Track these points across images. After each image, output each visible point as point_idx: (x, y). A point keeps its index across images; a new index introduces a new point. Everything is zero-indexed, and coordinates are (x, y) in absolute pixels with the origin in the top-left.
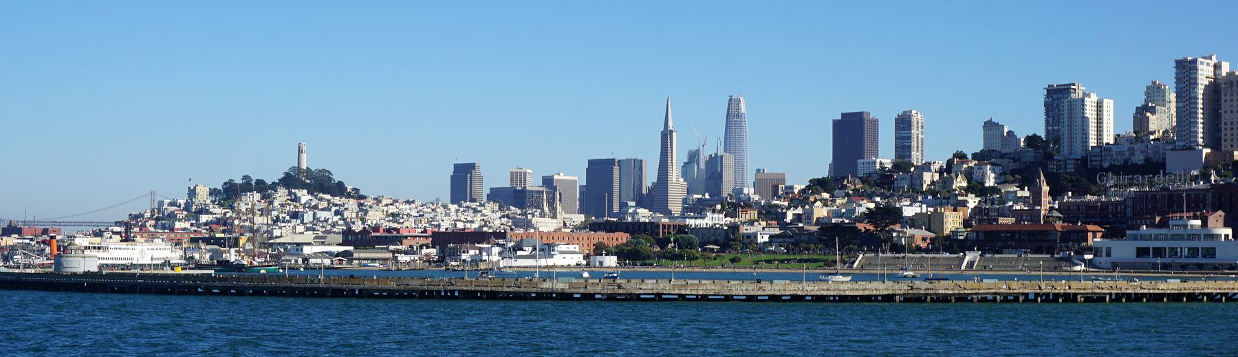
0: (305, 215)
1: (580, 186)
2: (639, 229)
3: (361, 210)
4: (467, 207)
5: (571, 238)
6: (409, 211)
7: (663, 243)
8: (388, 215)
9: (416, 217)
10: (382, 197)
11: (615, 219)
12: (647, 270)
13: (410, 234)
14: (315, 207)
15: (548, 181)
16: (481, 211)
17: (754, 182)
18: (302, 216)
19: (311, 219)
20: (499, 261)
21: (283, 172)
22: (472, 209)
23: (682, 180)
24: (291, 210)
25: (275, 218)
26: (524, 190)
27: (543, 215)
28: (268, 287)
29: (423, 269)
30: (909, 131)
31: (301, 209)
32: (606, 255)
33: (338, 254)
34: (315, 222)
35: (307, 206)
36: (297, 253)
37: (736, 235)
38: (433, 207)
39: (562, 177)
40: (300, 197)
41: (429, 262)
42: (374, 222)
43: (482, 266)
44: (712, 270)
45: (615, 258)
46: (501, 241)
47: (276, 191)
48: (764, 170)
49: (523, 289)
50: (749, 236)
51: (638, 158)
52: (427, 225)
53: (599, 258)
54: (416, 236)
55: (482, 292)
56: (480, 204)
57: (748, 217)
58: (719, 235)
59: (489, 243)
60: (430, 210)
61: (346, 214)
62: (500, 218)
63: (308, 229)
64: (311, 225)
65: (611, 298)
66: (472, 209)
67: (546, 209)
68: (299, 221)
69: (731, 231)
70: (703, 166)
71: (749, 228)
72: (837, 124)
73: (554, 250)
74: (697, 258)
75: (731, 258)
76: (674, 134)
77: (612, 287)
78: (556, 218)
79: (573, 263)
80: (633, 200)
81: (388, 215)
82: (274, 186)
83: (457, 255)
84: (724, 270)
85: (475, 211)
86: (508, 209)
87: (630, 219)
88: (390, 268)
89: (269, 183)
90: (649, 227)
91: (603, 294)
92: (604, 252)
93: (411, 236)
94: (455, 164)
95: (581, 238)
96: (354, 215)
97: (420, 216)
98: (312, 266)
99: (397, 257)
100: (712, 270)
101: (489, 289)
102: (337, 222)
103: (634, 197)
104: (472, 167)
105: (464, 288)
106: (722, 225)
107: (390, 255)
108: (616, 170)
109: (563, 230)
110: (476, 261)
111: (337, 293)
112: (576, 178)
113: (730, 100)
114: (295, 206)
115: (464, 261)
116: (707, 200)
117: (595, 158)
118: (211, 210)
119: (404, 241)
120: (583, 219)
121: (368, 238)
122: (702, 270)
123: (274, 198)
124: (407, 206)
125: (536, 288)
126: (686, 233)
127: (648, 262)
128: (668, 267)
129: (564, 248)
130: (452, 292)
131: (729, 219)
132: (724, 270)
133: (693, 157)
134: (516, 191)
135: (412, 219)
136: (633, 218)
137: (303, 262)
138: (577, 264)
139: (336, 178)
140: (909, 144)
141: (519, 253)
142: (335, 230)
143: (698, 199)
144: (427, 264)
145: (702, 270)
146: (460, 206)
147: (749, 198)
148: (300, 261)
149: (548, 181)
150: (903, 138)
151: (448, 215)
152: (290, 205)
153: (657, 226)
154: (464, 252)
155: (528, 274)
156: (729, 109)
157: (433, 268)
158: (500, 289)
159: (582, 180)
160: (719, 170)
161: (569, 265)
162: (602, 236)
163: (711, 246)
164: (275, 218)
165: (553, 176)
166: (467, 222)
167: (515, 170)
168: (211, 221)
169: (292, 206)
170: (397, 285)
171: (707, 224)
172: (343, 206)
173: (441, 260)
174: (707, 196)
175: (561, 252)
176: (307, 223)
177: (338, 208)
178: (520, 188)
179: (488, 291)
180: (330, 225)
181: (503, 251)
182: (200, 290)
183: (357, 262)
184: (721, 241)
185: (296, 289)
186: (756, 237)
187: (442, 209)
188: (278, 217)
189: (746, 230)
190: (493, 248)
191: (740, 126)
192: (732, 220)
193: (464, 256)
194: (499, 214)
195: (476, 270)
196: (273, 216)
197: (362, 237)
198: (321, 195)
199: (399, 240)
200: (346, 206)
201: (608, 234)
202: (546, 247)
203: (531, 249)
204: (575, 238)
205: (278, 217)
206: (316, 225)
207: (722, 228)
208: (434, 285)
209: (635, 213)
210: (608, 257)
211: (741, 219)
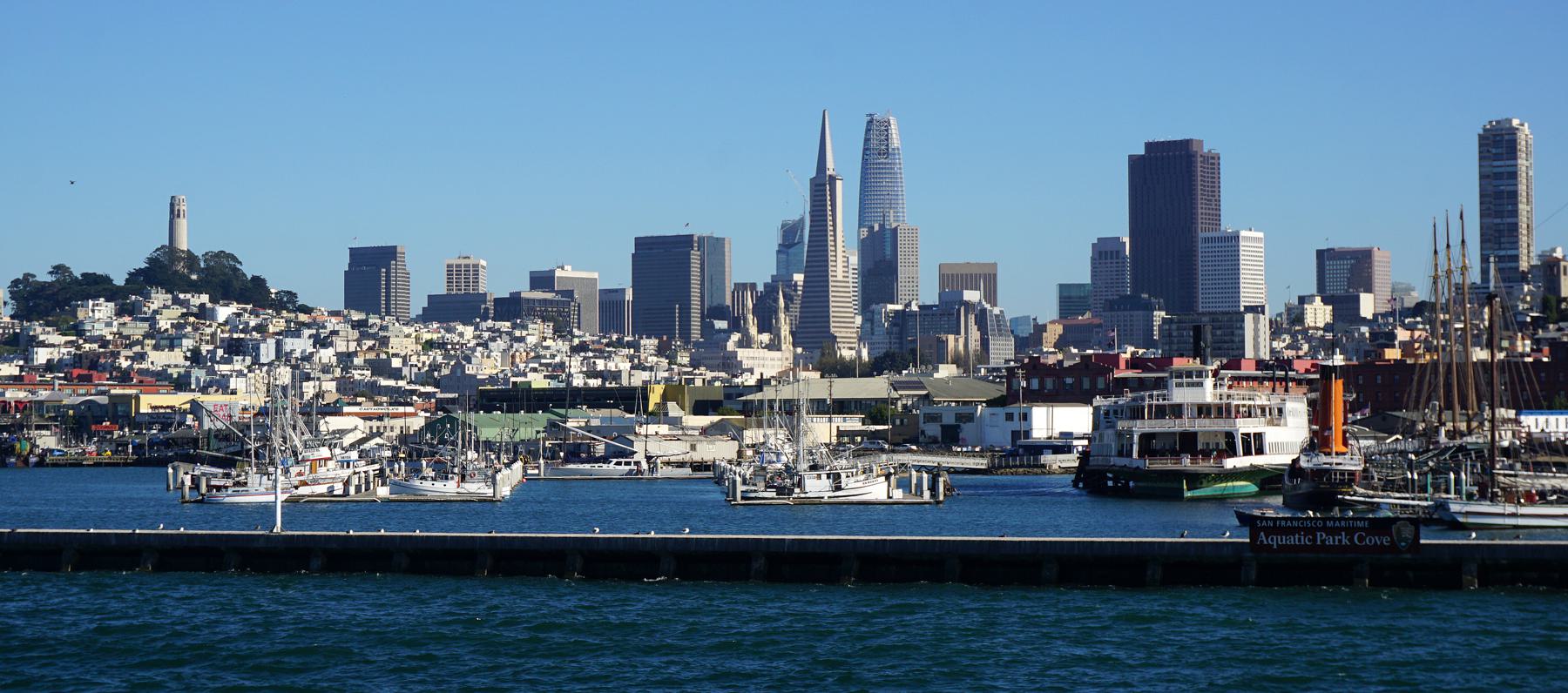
30: (1512, 162)
72: (1135, 163)
76: (839, 183)
78: (779, 349)
104: (386, 255)
108: (695, 255)
112: (596, 275)
113: (870, 122)
117: (650, 234)
118: (42, 338)
139: (249, 270)
140: (1512, 188)
150: (1498, 176)
156: (867, 140)
160: (888, 251)
165: (553, 271)
167: (455, 262)
168: (60, 360)
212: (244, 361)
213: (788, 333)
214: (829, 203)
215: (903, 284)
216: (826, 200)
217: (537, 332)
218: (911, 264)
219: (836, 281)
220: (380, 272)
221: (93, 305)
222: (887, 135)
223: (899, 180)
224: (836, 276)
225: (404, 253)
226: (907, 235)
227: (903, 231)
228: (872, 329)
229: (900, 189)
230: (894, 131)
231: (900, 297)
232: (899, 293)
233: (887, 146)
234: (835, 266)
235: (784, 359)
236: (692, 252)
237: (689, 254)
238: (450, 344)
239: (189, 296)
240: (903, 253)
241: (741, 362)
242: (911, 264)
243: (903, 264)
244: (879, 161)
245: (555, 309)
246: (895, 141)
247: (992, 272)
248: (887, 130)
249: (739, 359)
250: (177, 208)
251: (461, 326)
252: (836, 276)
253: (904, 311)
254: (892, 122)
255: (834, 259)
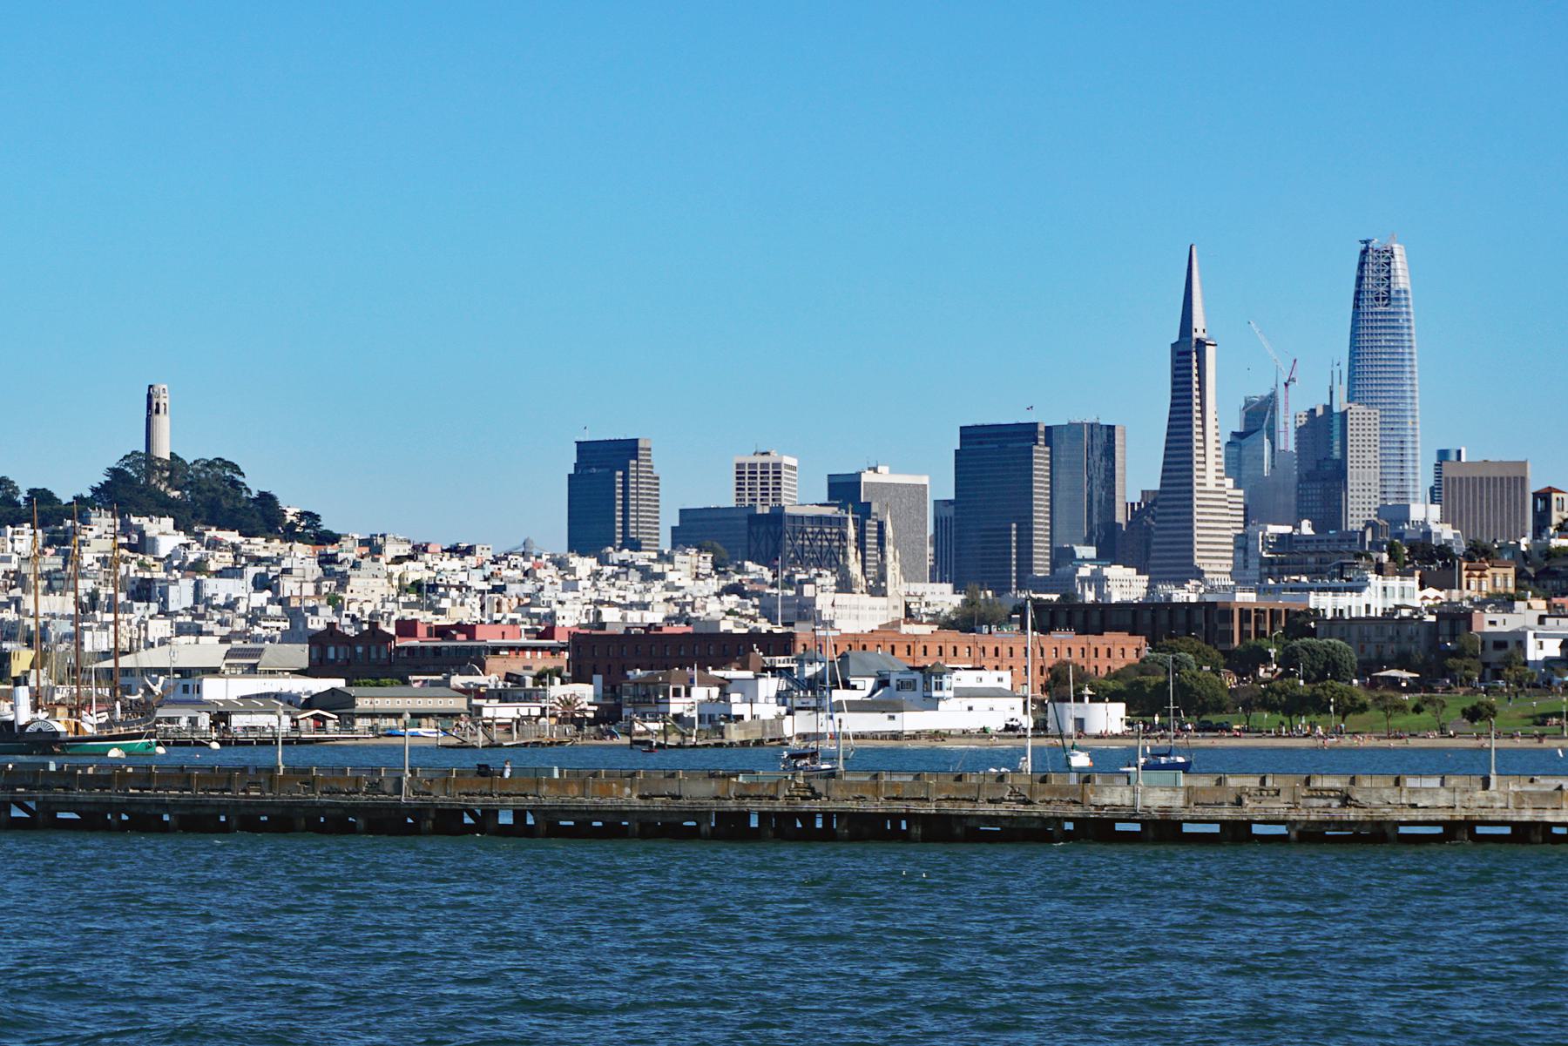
0: (172, 590)
1: (938, 504)
2: (1171, 625)
3: (328, 574)
4: (622, 564)
5: (977, 653)
6: (463, 577)
7: (1246, 662)
8: (403, 590)
9: (482, 592)
10: (383, 536)
11: (1055, 597)
12: (1218, 743)
13: (508, 641)
14: (199, 567)
15: (844, 489)
16: (661, 576)
17: (1432, 490)
18: (164, 593)
19: (189, 602)
20: (779, 718)
21: (103, 469)
22: (638, 568)
23: (1229, 482)
24: (132, 575)
25: (85, 599)
26: (777, 516)
27: (845, 585)
28: (237, 805)
29: (560, 743)
31: (159, 574)
32: (1093, 699)
33: (311, 702)
34: (201, 609)
35: (176, 563)
36: (185, 697)
37: (1463, 638)
38: (527, 565)
39: (885, 476)
40: (154, 539)
41: (579, 723)
42: (368, 609)
43: (734, 734)
44: (1413, 742)
45: (1119, 709)
46: (781, 662)
47: (85, 521)
48: (1459, 452)
49: (1039, 809)
50: (1500, 643)
51: (1104, 422)
52: (518, 616)
53: (1072, 710)
54: (524, 648)
55: (910, 817)
56: (661, 554)
57: (1486, 586)
58: (1411, 638)
59: (744, 667)
60: (518, 574)
61: (288, 586)
62: (718, 595)
63: (181, 630)
64: (189, 619)
65: (1312, 835)
66: (638, 568)
67: (855, 568)
68: (154, 607)
69: (1445, 627)
70: (1288, 441)
71: (1499, 617)
73: (939, 687)
74: (1363, 708)
75: (1467, 706)
76: (1210, 351)
77: (1323, 802)
78: (884, 595)
79: (996, 723)
80: (1088, 542)
81: (403, 590)
82: (81, 508)
83: (657, 702)
84: (1447, 743)
85: (647, 575)
86: (740, 570)
87: (1090, 597)
88: (469, 739)
89: (66, 498)
90: (1200, 617)
91: (1291, 824)
92: (1087, 691)
93: (511, 648)
94: (578, 443)
95: (1005, 651)
96: (309, 589)
97: (495, 589)
98: (241, 736)
99: (479, 709)
100: (1413, 742)
101: (931, 808)
102: (263, 610)
103: (1091, 533)
104: (627, 450)
105: (853, 806)
106: (1416, 610)
107: (460, 704)
108: (1041, 454)
109: (905, 629)
110: (716, 719)
111: (447, 822)
113: (1364, 252)
114: (142, 565)
115: (678, 718)
116: (1308, 540)
119: (491, 662)
120: (957, 600)
121: (383, 656)
122: (1384, 743)
123: (83, 543)
124: (456, 563)
125: (1081, 804)
126: (1312, 633)
127: (1215, 719)
128: (1278, 736)
129: (968, 679)
130: (809, 817)
131: (1431, 592)
132: (1447, 743)
133: (1259, 416)
134: (754, 519)
135: (473, 601)
136: (1099, 593)
137: (214, 724)
138: (1008, 728)
139: (255, 483)
141: (839, 695)
142: (257, 630)
143: (1281, 536)
144: (570, 729)
145: (1384, 743)
146: (603, 561)
147: (1428, 534)
148: (204, 721)
149: (844, 489)
151: (571, 586)
152: (126, 561)
153: (1226, 614)
154: (677, 693)
155: (992, 758)
156: (1360, 279)
157: (588, 739)
158: (966, 808)
159: (944, 487)
160: (1337, 454)
161: (984, 730)
162: (1065, 645)
163: (1393, 673)
164: (85, 599)
165: (859, 475)
166: (631, 606)
167: (749, 459)
169: (134, 566)
170: (642, 797)
171: (1368, 607)
172: (278, 563)
173: (608, 716)
174: (1306, 528)
175: (961, 693)
176: (177, 613)
177: (262, 569)
178: (767, 510)
179: (927, 817)
180: (244, 616)
181: (789, 690)
182: (16, 813)
183: (367, 722)
184: (1418, 658)
185: (262, 806)
186: (1521, 644)
187: (552, 569)
188: (94, 596)
189: (1490, 622)
190: (761, 682)
191: (1393, 326)
192: (1442, 595)
193: (677, 706)
194: (715, 584)
195: (717, 745)
196: (81, 592)
197: (367, 651)
198: (213, 532)
199: (472, 659)
200: (286, 564)
201: (1083, 638)
202: (917, 675)
203: (870, 683)
204: (990, 650)
205: (94, 596)
206: (202, 617)
207: (1421, 618)
208: (759, 797)
209: (1099, 581)
210: (1100, 706)
211: (1467, 593)
212: (148, 608)
213: (897, 572)
214: (1195, 379)
215: (1356, 493)
216: (1191, 375)
217: (687, 566)
218: (1367, 465)
219: (1206, 492)
220: (614, 476)
221: (13, 533)
222: (1389, 271)
223: (1406, 337)
224: (1204, 484)
225: (649, 449)
226: (1361, 422)
227: (1355, 416)
228: (1246, 561)
229: (1407, 350)
230: (1399, 265)
231: (1350, 512)
232: (1350, 506)
233: (1389, 286)
234: (1203, 470)
235: (891, 608)
236: (1035, 448)
237: (1031, 451)
238: (443, 586)
239: (145, 520)
240: (1355, 449)
241: (820, 612)
242: (1367, 465)
243: (1355, 464)
244: (1375, 309)
245: (835, 531)
246: (1401, 280)
247: (1519, 475)
248: (1389, 264)
249: (818, 607)
250: (155, 401)
251: (577, 558)
252: (1204, 484)
253: (1291, 535)
254: (1396, 252)
255: (1202, 459)
